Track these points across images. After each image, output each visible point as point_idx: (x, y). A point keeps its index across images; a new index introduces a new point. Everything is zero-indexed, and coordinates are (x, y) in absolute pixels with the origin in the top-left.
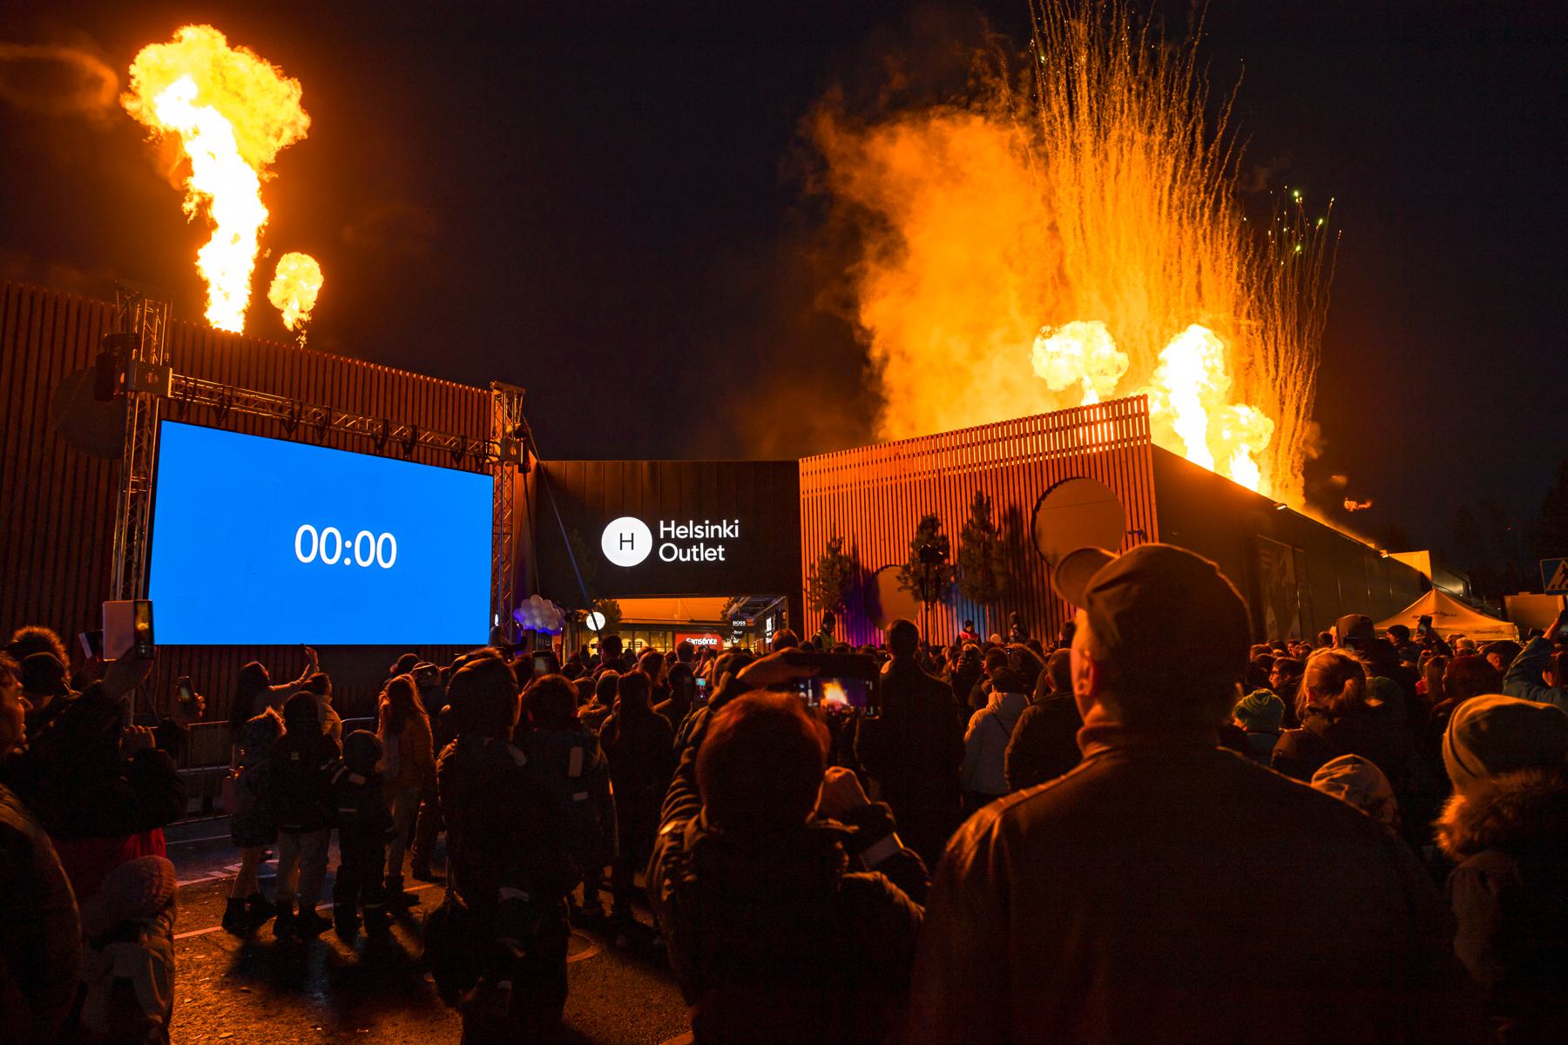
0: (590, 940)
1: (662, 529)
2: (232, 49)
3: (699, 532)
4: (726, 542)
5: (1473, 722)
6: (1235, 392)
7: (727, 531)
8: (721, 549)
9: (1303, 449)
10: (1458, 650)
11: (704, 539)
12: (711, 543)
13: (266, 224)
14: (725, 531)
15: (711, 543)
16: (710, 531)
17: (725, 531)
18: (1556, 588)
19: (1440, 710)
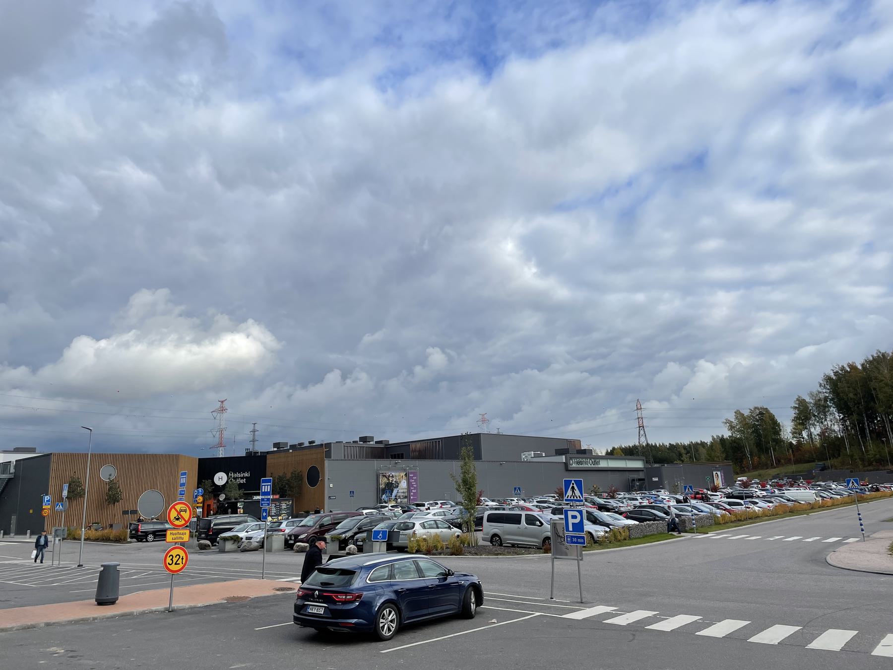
0: (578, 466)
1: (230, 475)
2: (828, 379)
3: (238, 475)
4: (246, 478)
5: (299, 546)
6: (470, 553)
7: (247, 475)
8: (245, 480)
9: (772, 426)
10: (813, 418)
11: (240, 477)
12: (242, 478)
13: (746, 413)
14: (246, 475)
15: (242, 478)
16: (242, 475)
17: (246, 475)
18: (569, 498)
19: (317, 535)
